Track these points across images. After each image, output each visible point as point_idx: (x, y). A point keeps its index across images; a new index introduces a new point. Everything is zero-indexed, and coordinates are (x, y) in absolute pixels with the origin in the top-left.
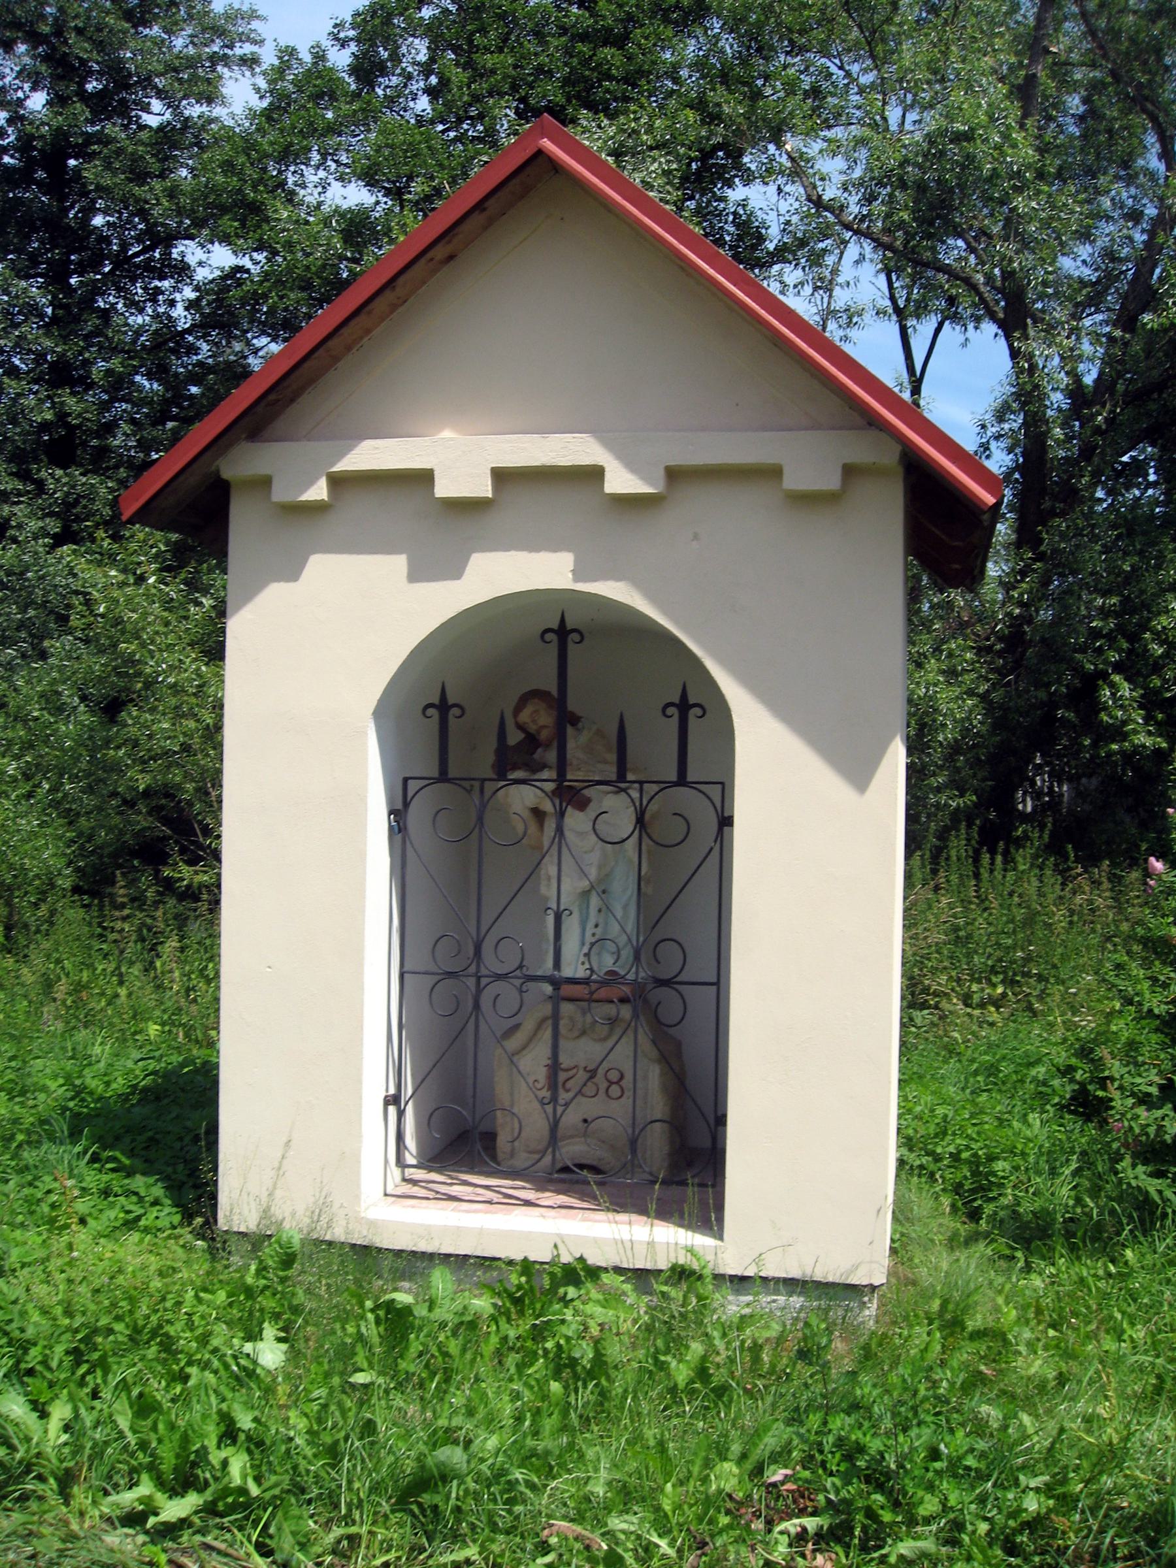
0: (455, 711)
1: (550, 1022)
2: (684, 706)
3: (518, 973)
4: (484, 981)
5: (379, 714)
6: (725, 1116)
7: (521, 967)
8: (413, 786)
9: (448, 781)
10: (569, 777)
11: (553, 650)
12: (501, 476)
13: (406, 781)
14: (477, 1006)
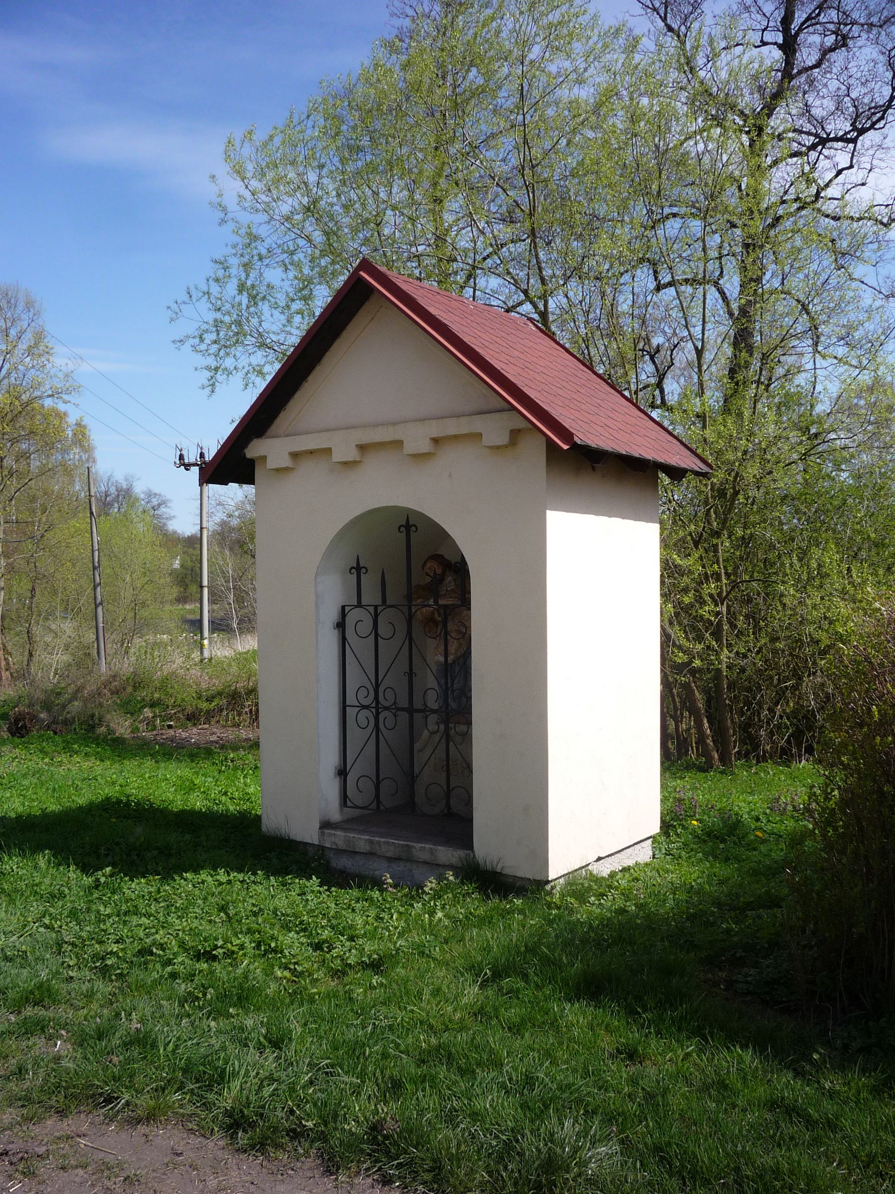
7: (395, 703)
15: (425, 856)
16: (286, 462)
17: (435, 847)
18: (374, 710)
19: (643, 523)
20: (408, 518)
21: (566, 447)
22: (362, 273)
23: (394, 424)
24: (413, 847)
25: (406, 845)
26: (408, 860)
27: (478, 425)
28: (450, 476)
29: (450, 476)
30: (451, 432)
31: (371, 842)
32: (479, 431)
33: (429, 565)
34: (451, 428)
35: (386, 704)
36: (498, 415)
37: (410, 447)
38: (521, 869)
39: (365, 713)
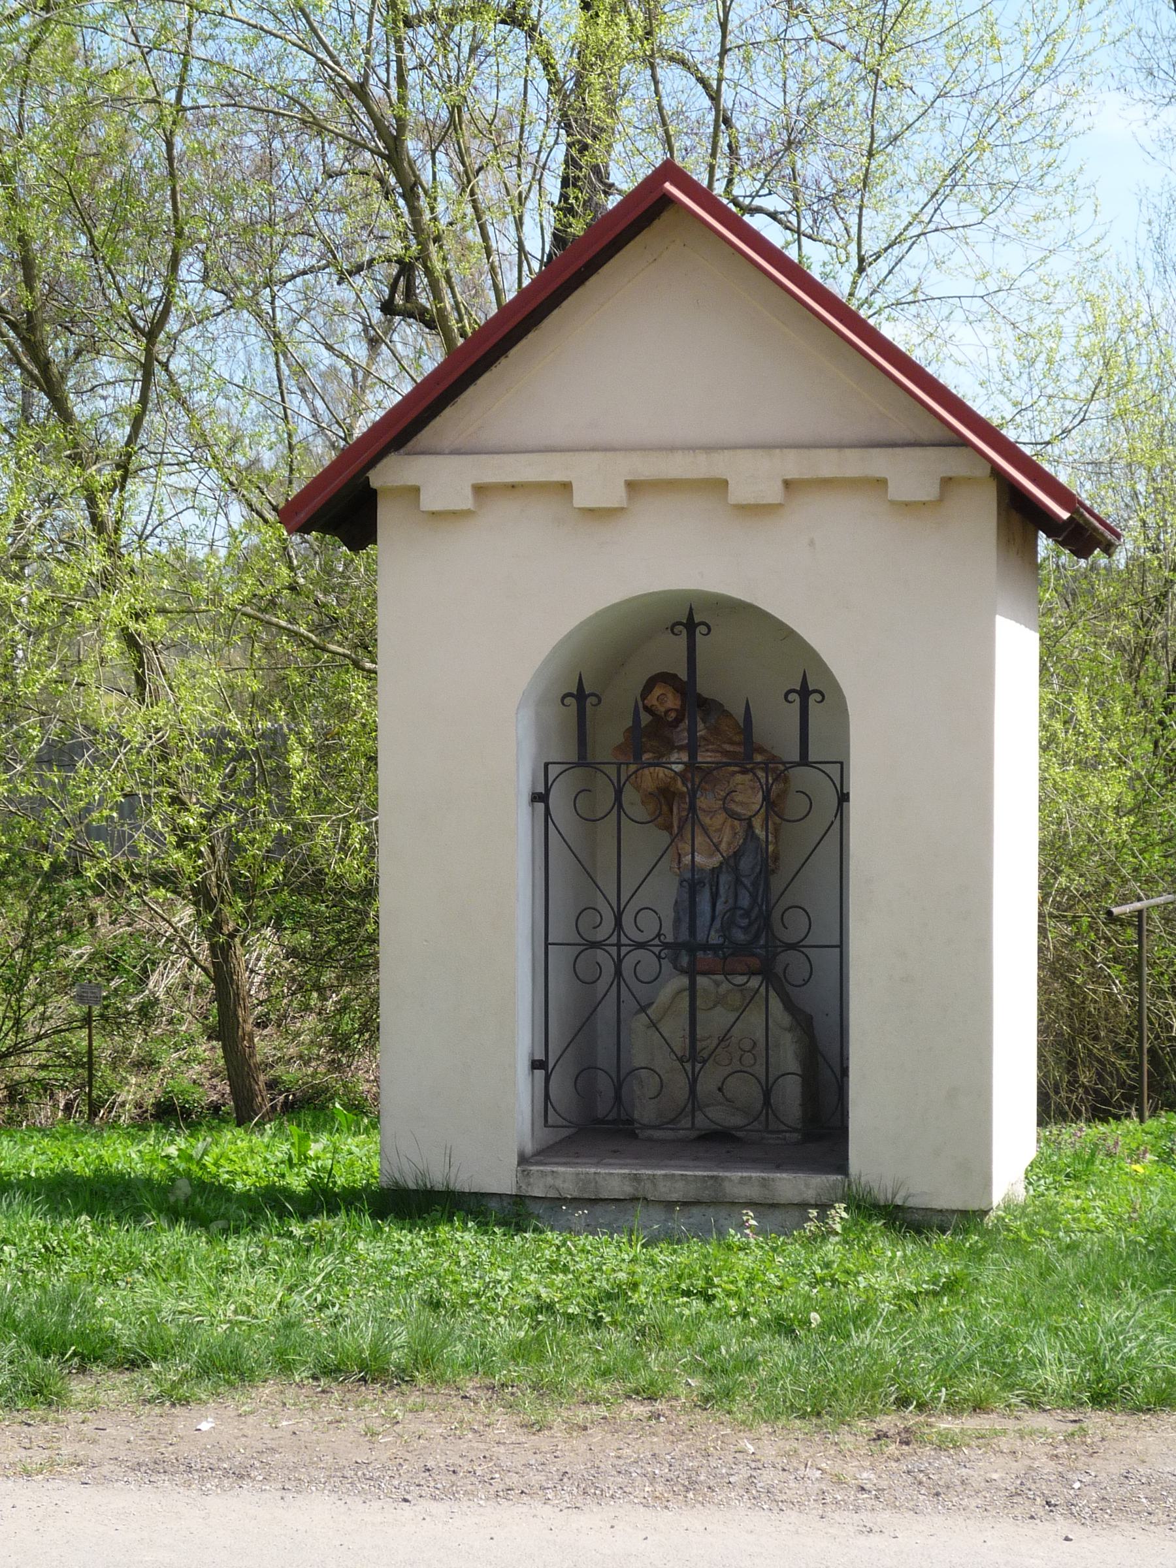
0: (591, 700)
1: (686, 993)
2: (804, 692)
3: (656, 942)
4: (624, 950)
5: (375, 542)
6: (847, 1068)
7: (659, 935)
8: (554, 771)
9: (588, 765)
10: (700, 759)
11: (682, 641)
12: (633, 487)
13: (546, 765)
14: (618, 973)
15: (753, 1192)
16: (465, 501)
17: (771, 1175)
18: (613, 950)
19: (1013, 622)
20: (691, 609)
21: (1065, 515)
22: (668, 186)
23: (709, 449)
24: (723, 1179)
25: (712, 1177)
26: (714, 1203)
27: (878, 463)
28: (812, 543)
29: (812, 543)
30: (827, 472)
31: (636, 1178)
32: (883, 475)
33: (657, 691)
34: (827, 465)
35: (640, 938)
36: (918, 452)
37: (739, 493)
38: (948, 1199)
39: (791, 937)
